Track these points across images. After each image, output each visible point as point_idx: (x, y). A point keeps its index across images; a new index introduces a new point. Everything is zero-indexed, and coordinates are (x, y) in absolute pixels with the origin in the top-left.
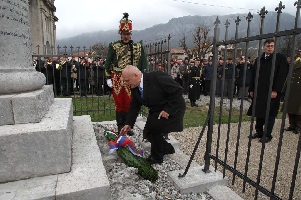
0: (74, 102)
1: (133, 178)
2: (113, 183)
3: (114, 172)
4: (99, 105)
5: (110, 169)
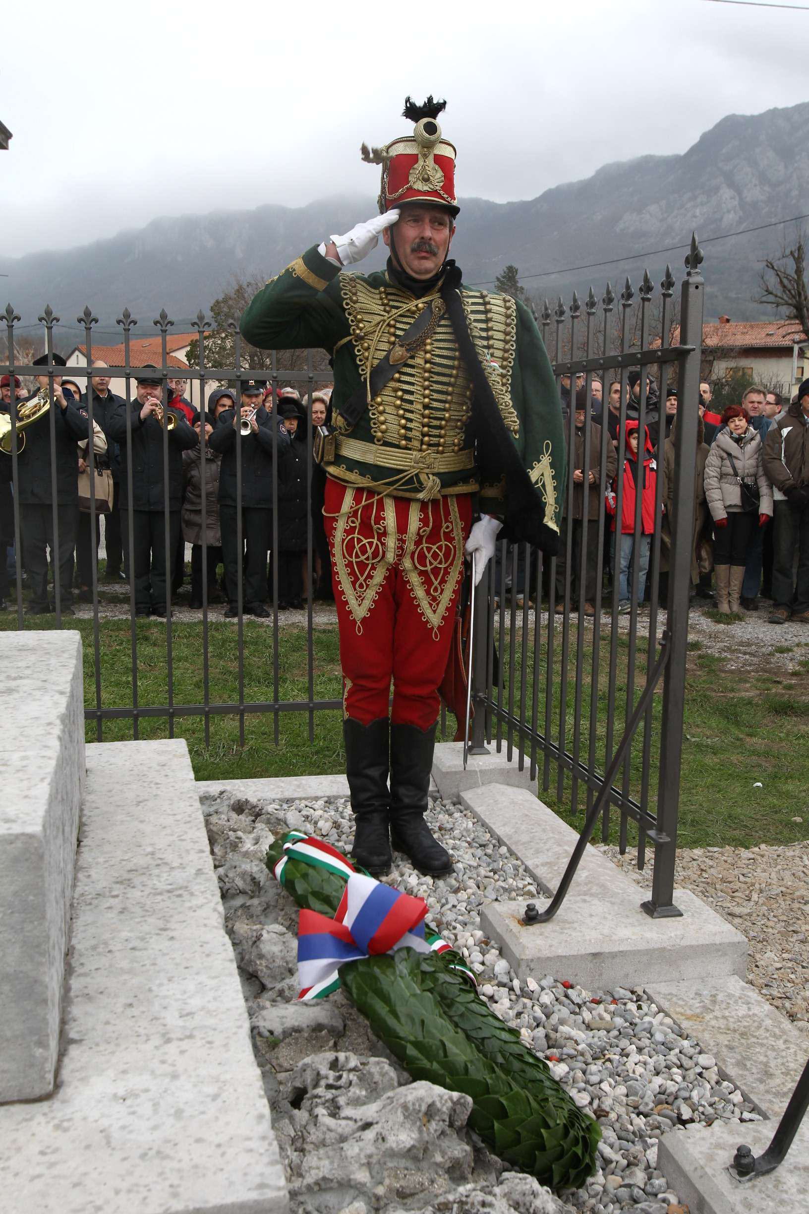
0: (91, 650)
1: (438, 1158)
2: (309, 1179)
3: (321, 1111)
4: (242, 675)
5: (295, 1088)
